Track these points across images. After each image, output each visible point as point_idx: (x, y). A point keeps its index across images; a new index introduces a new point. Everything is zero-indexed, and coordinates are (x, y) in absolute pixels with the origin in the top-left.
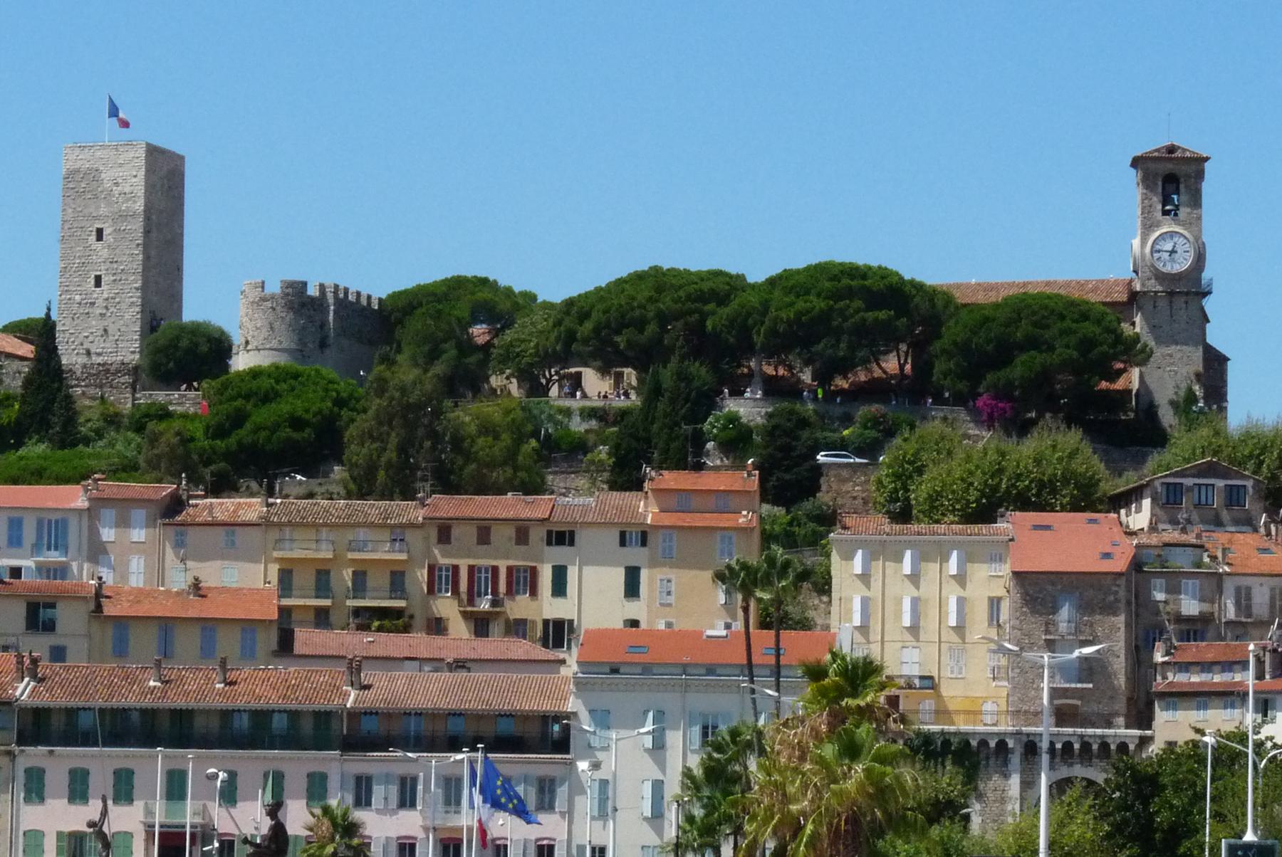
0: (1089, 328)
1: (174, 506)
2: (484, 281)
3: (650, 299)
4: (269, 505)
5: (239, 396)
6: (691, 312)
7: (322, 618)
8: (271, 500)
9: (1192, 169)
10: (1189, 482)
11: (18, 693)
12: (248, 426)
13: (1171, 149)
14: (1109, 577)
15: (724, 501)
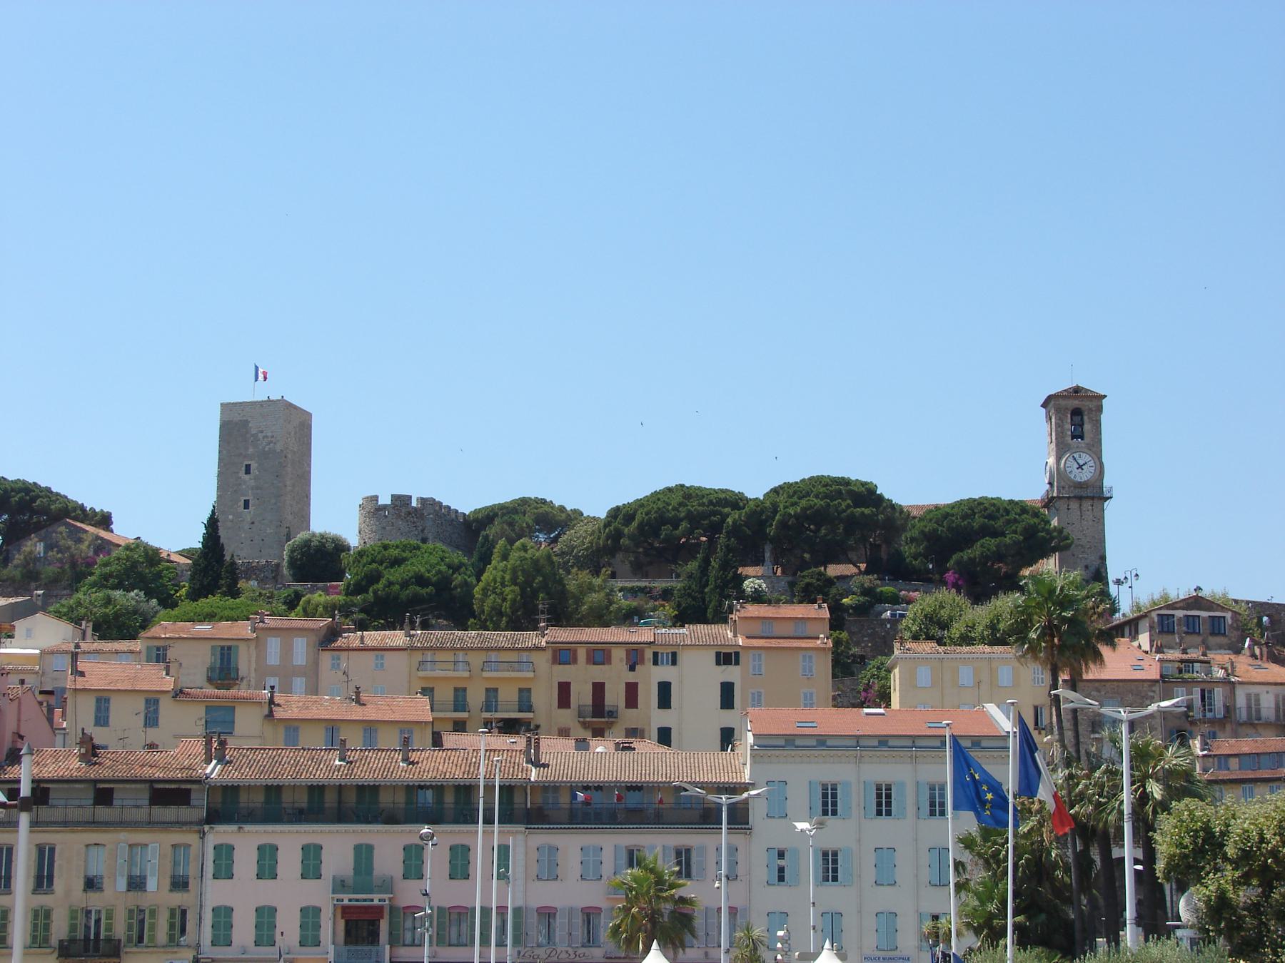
0: (1029, 520)
1: (332, 634)
2: (543, 502)
3: (680, 504)
4: (410, 636)
5: (373, 561)
6: (714, 513)
7: (460, 727)
8: (412, 632)
9: (1092, 405)
10: (1180, 614)
11: (208, 771)
12: (383, 582)
13: (1077, 390)
14: (1146, 685)
15: (800, 630)
